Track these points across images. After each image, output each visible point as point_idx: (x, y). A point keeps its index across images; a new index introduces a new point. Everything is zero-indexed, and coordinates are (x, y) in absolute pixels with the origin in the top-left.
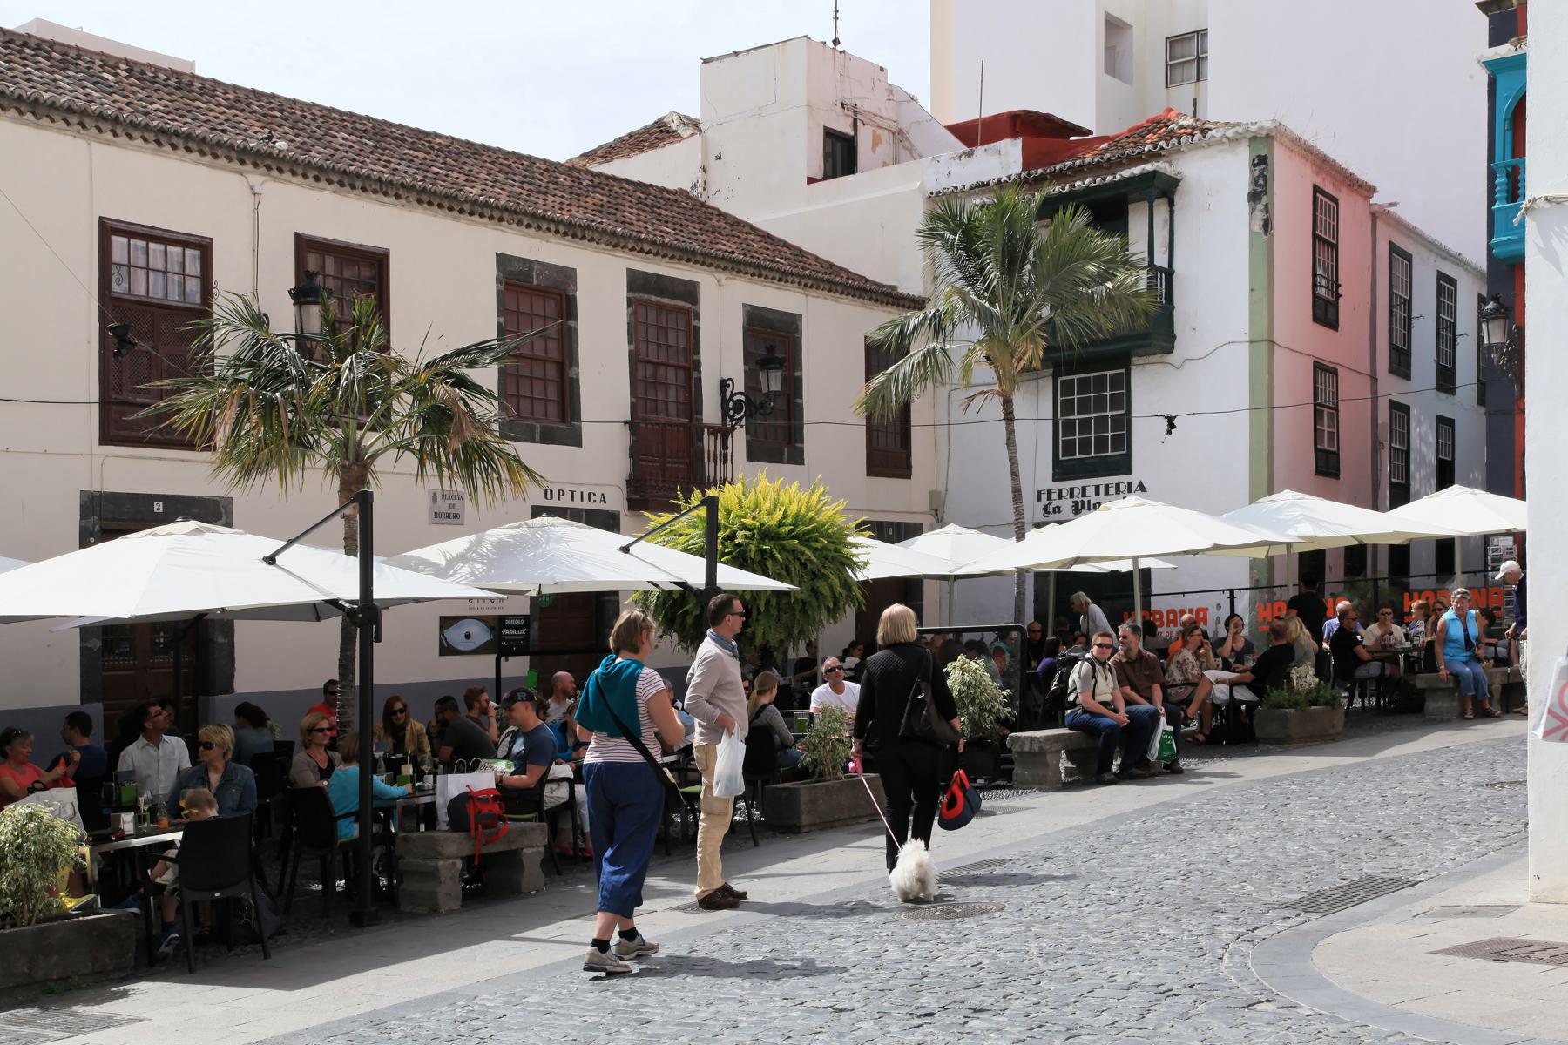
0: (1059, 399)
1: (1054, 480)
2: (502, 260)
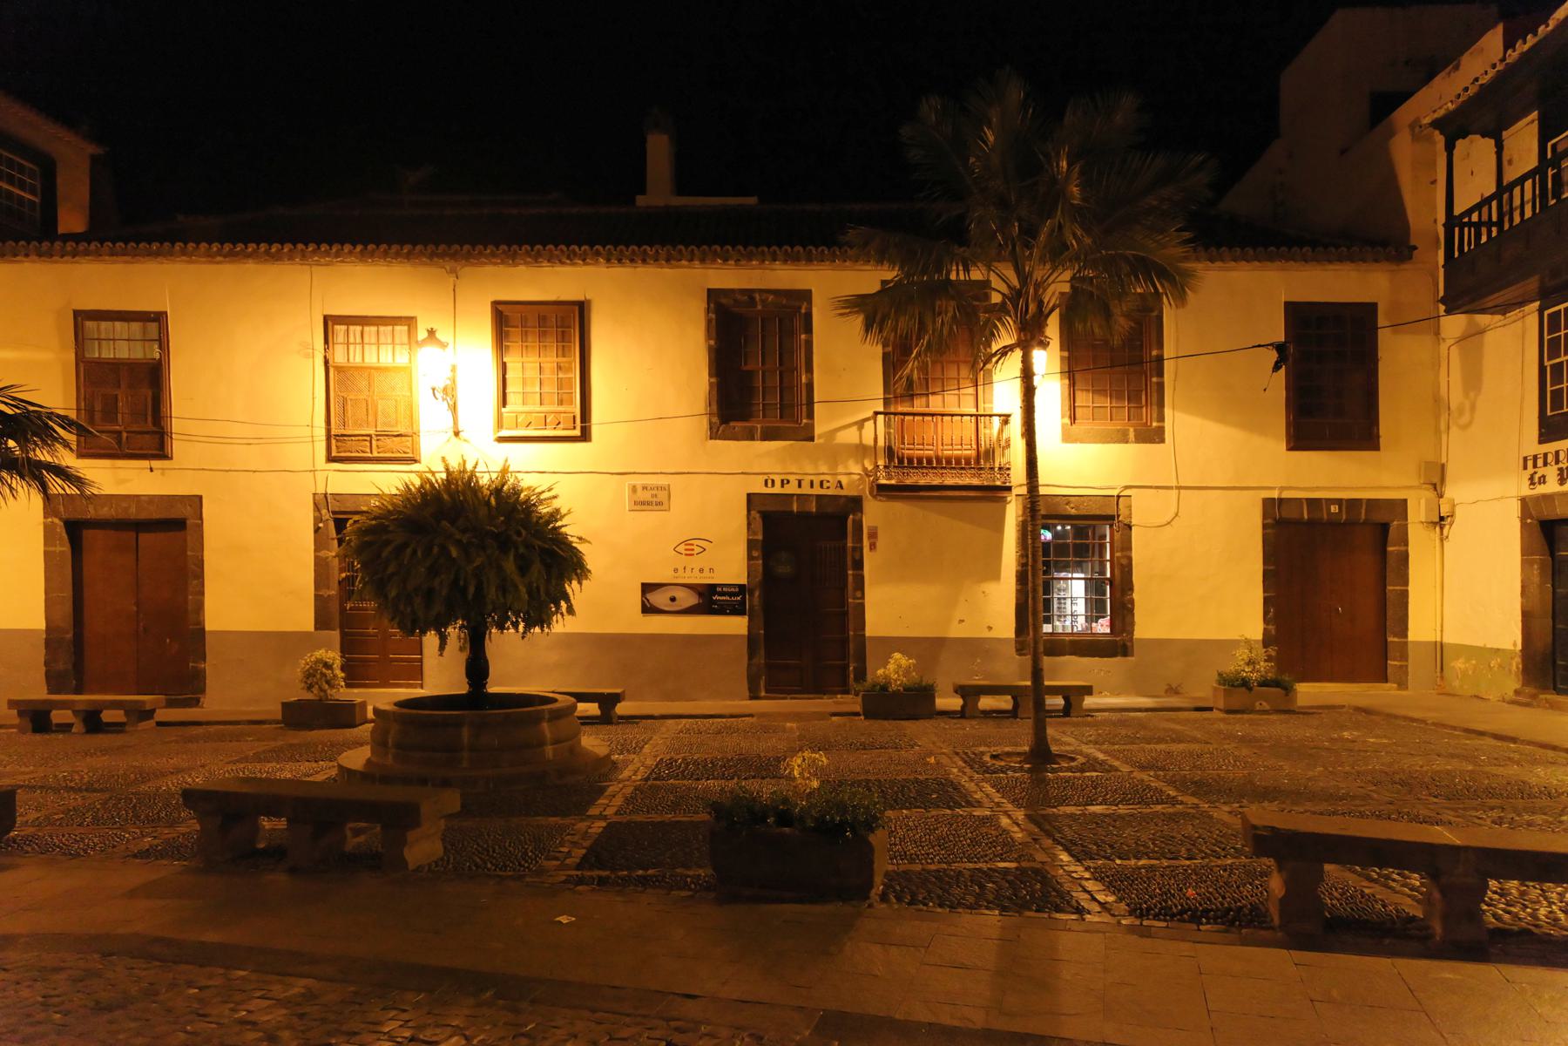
0: (1546, 337)
1: (1540, 442)
2: (713, 295)
